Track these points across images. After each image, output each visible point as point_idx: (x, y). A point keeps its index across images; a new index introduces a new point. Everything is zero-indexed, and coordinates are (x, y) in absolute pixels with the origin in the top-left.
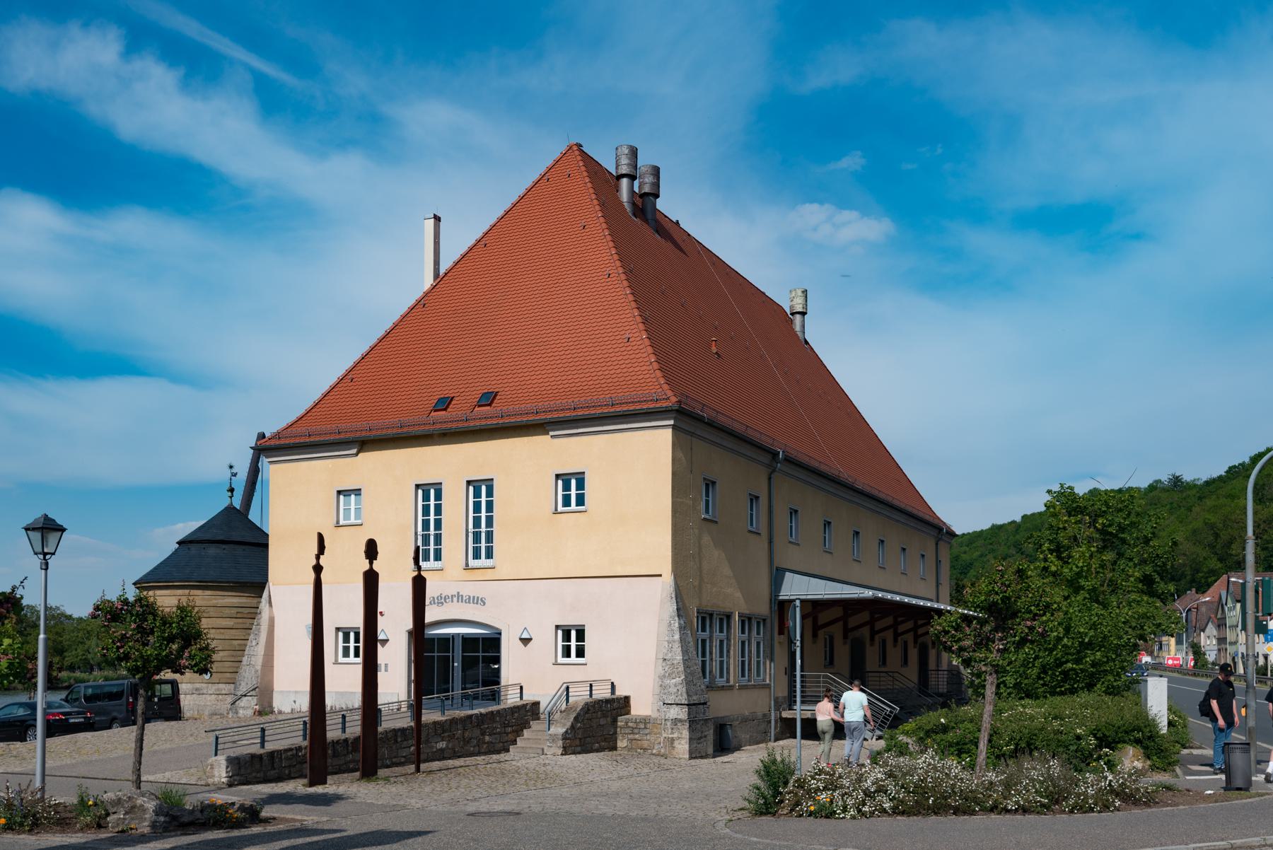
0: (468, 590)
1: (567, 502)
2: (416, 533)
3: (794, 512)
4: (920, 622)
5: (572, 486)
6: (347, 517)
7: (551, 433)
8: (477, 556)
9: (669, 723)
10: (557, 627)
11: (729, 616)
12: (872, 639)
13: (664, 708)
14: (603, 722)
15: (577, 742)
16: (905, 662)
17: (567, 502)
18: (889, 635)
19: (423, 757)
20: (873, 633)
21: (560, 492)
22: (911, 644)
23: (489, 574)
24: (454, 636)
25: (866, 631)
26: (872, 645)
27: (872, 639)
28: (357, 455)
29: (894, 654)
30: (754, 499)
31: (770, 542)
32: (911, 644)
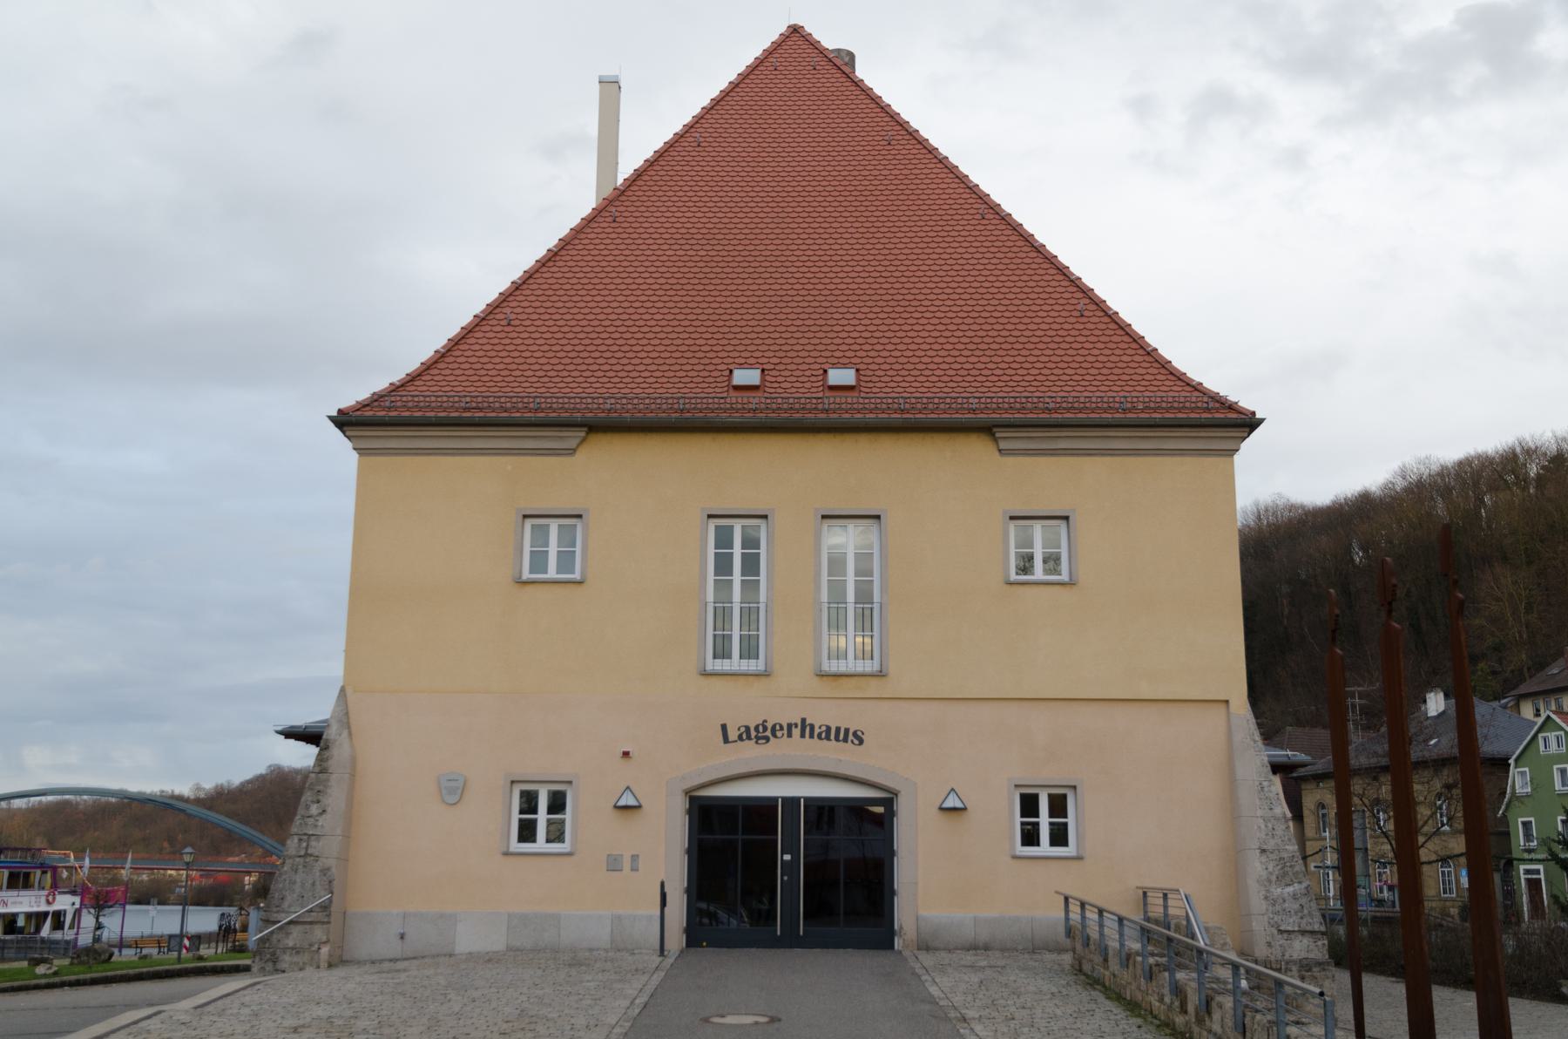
7: (1003, 445)
9: (1294, 968)
13: (1280, 940)
24: (791, 803)
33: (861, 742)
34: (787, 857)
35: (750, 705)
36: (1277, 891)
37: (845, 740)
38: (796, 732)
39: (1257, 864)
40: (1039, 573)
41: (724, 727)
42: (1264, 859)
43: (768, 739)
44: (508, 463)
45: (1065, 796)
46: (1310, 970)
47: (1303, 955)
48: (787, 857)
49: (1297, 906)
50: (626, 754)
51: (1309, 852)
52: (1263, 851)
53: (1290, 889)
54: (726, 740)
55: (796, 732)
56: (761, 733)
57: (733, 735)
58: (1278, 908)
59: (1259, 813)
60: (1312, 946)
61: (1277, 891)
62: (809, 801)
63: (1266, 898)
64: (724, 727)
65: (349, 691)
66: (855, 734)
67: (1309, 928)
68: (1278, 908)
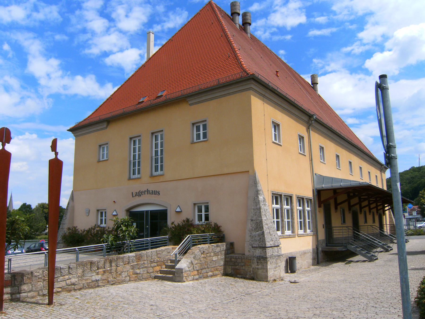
0: (151, 188)
1: (198, 136)
2: (130, 161)
3: (322, 148)
4: (379, 204)
5: (200, 127)
6: (103, 157)
7: (190, 103)
8: (156, 170)
9: (255, 259)
10: (195, 204)
11: (291, 197)
12: (361, 211)
13: (253, 250)
14: (215, 258)
15: (196, 272)
16: (374, 222)
17: (198, 136)
18: (367, 209)
19: (263, 246)
20: (361, 208)
21: (195, 133)
22: (375, 213)
23: (162, 179)
24: (147, 212)
25: (357, 207)
26: (361, 213)
27: (361, 211)
28: (107, 127)
29: (370, 218)
30: (301, 138)
31: (311, 160)
32: (375, 213)
33: (159, 194)
34: (147, 227)
35: (137, 187)
36: (254, 233)
37: (156, 194)
38: (146, 193)
39: (250, 225)
40: (202, 139)
41: (132, 193)
42: (252, 223)
43: (140, 195)
44: (96, 134)
45: (202, 206)
46: (260, 260)
47: (259, 255)
48: (147, 227)
49: (259, 238)
50: (114, 202)
51: (339, 201)
52: (252, 220)
53: (258, 233)
54: (133, 197)
55: (146, 193)
56: (139, 194)
57: (134, 195)
58: (253, 239)
59: (253, 207)
60: (262, 252)
61: (254, 233)
62: (151, 211)
63: (250, 236)
64: (132, 193)
65: (74, 193)
66: (140, 195)
67: (261, 246)
68: (253, 239)
